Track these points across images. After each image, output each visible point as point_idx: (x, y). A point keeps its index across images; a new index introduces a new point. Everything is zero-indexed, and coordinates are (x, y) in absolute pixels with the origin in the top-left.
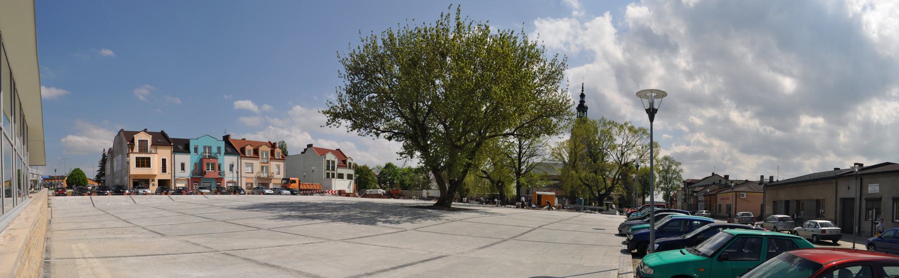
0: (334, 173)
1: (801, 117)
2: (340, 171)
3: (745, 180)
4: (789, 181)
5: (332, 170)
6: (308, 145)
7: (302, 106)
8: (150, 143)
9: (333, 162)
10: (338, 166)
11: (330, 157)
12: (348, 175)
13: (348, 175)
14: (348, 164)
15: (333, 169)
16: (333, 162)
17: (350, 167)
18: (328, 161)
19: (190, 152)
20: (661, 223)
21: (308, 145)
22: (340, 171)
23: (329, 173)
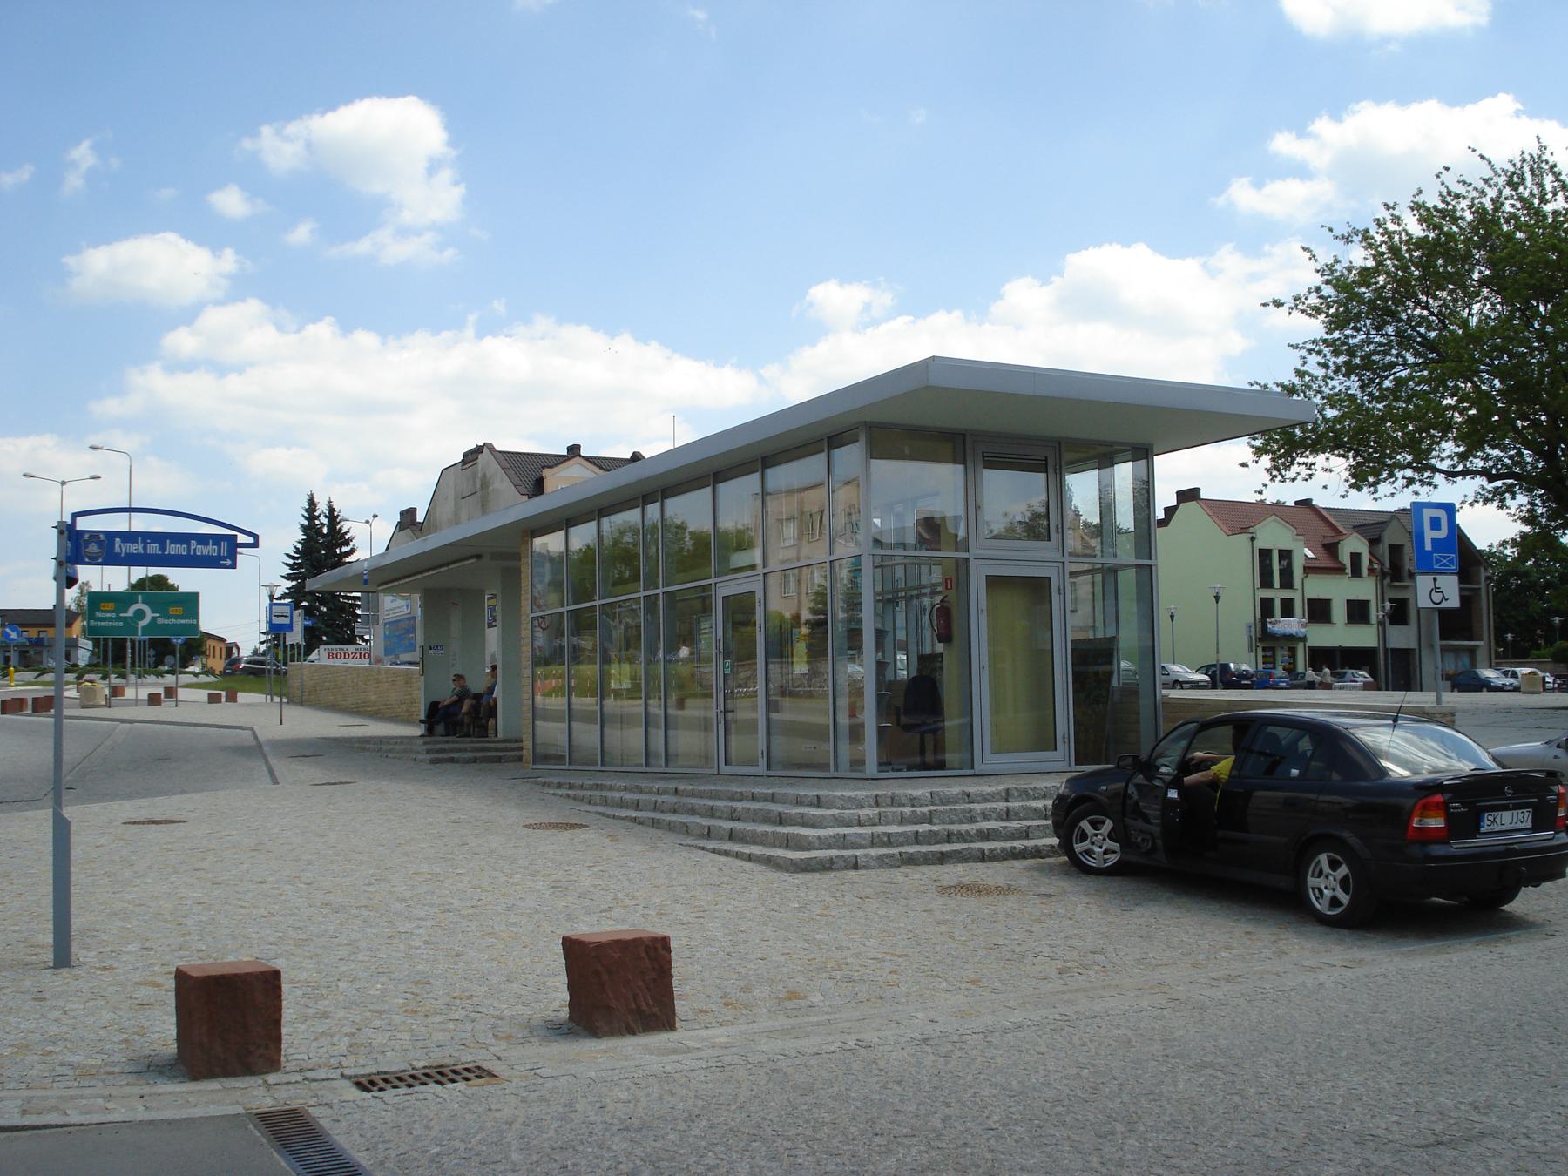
0: (1291, 600)
1: (328, 319)
2: (1318, 587)
3: (54, 583)
4: (1226, 408)
5: (1282, 586)
6: (1178, 493)
7: (845, 279)
8: (163, 696)
9: (1286, 555)
10: (1308, 570)
11: (1274, 536)
12: (1351, 604)
13: (1351, 604)
14: (1346, 561)
15: (1287, 582)
16: (1286, 555)
17: (1356, 572)
18: (1265, 554)
19: (1280, 551)
20: (1229, 695)
21: (1178, 493)
22: (1318, 587)
23: (1271, 600)
